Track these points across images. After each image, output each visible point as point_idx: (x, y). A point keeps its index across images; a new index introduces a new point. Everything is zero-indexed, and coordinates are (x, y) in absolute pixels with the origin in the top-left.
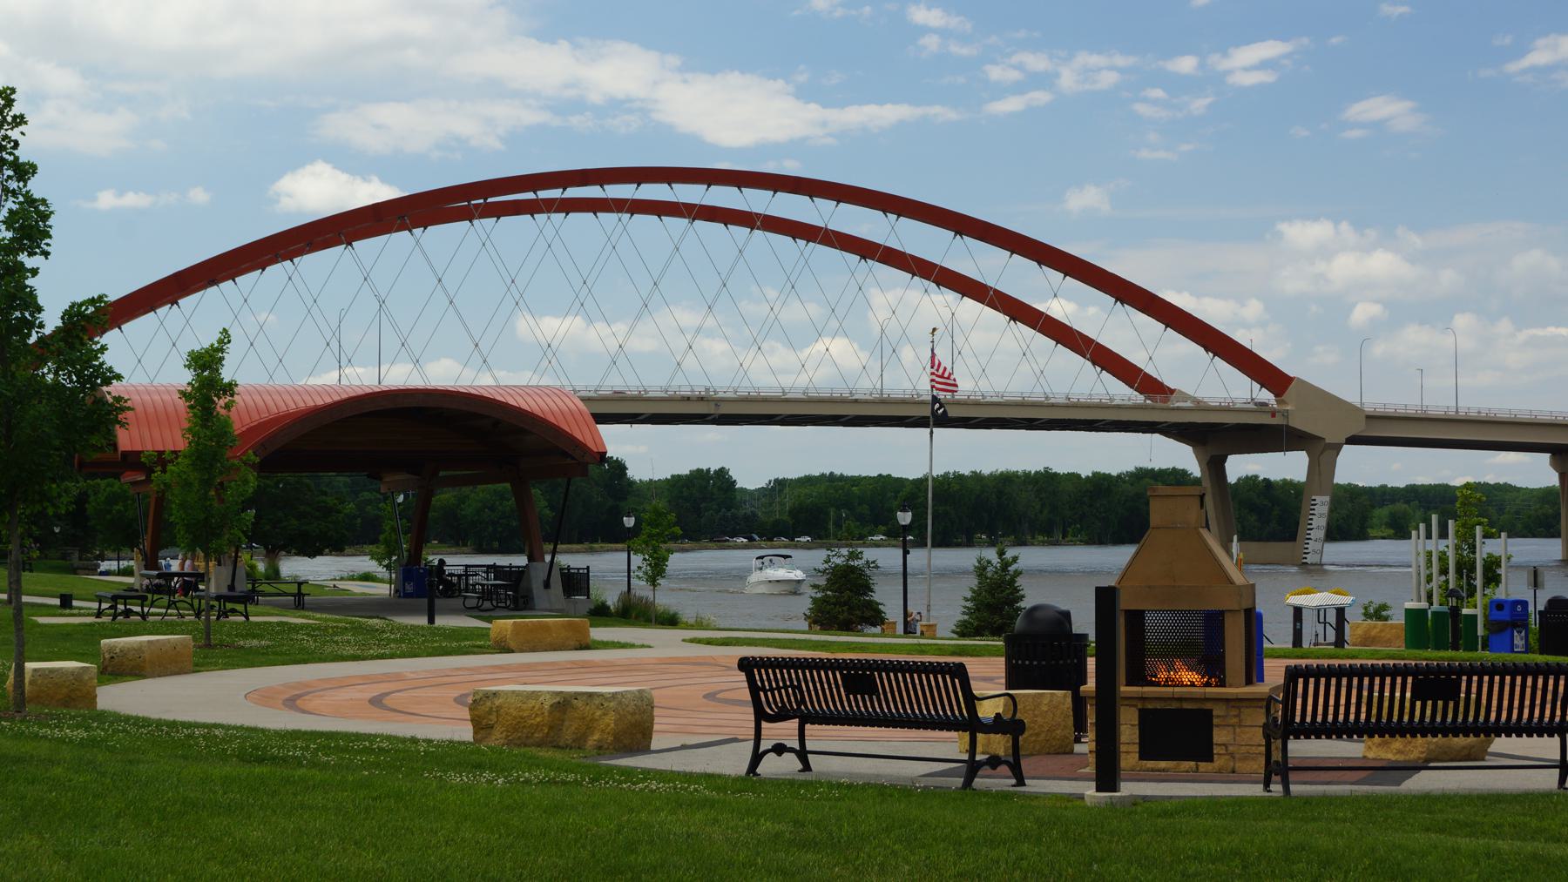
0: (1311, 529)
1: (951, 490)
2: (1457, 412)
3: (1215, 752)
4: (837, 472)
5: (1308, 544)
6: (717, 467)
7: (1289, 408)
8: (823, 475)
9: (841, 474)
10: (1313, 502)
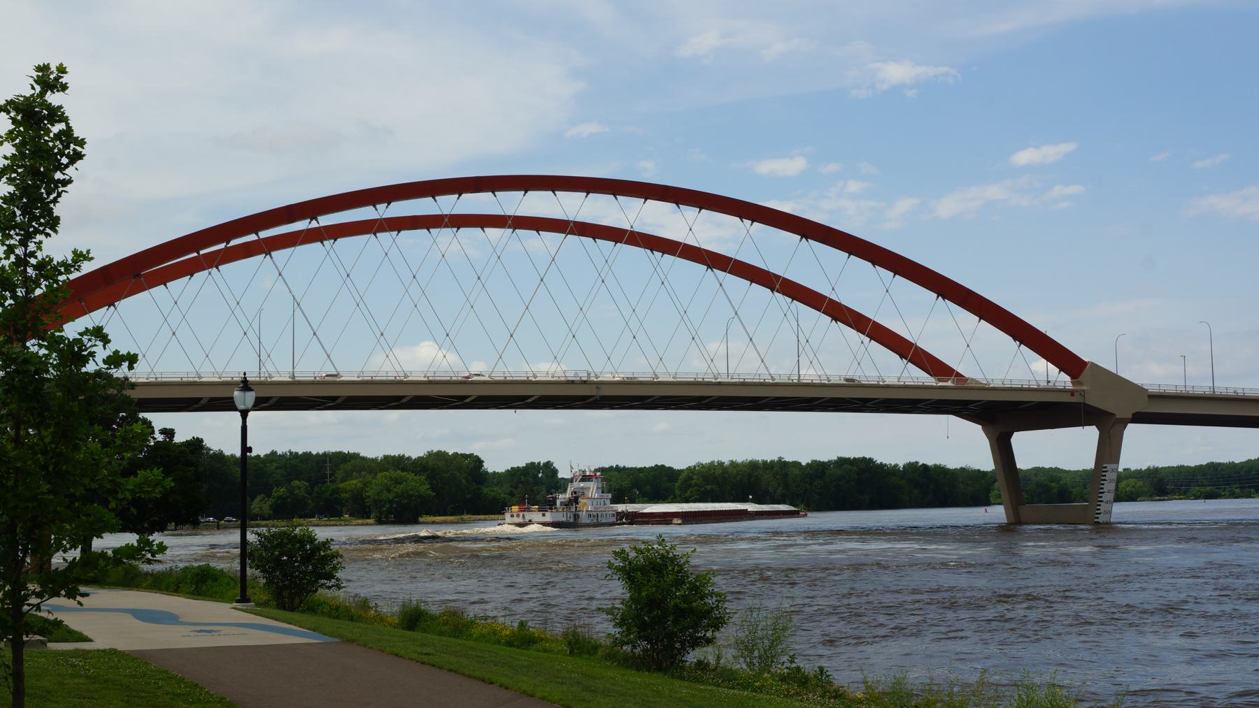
0: (1103, 493)
2: (1214, 391)
4: (621, 465)
5: (1100, 505)
6: (545, 461)
7: (1084, 388)
8: (612, 467)
9: (617, 466)
10: (1104, 470)
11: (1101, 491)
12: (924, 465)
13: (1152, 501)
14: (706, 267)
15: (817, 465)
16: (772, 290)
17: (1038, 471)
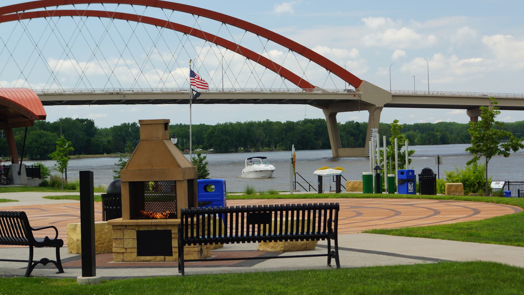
1: (228, 129)
2: (429, 93)
3: (173, 251)
7: (361, 93)
8: (177, 125)
9: (185, 124)
10: (371, 131)
12: (357, 123)
14: (183, 33)
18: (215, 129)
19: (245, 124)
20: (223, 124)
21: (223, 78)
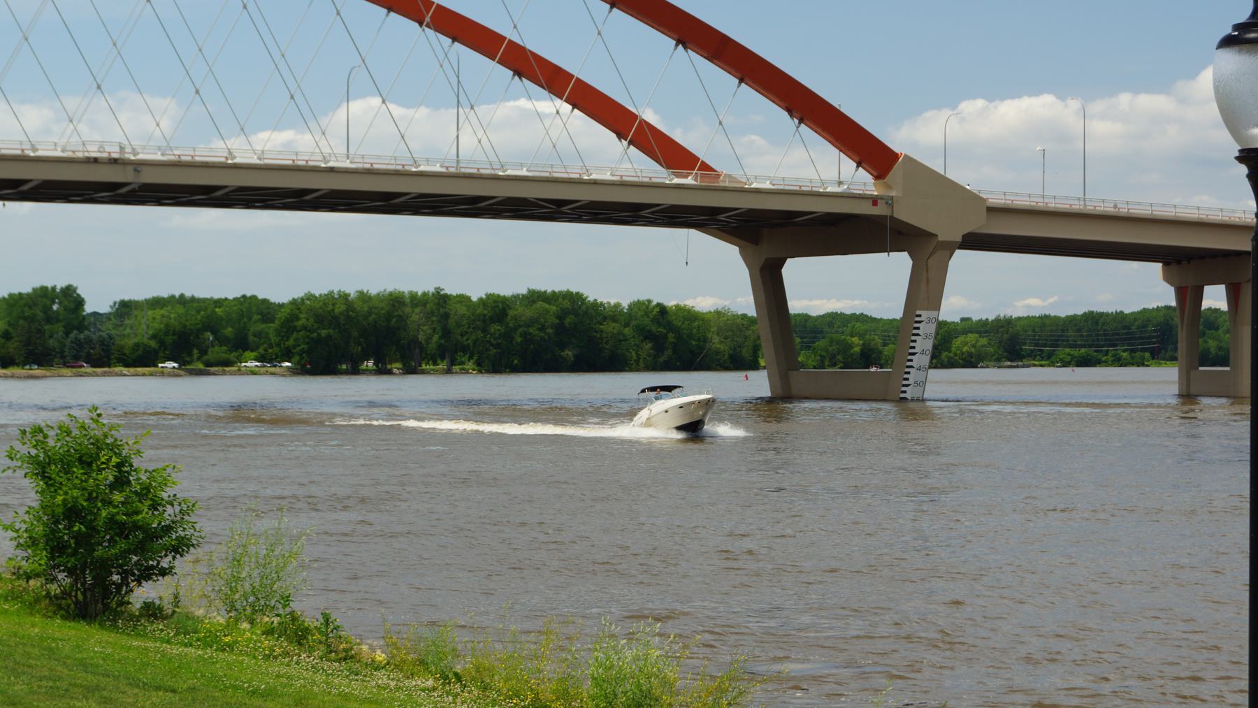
0: (914, 354)
4: (188, 294)
7: (893, 194)
8: (173, 297)
10: (917, 319)
11: (911, 351)
13: (999, 367)
15: (495, 302)
16: (421, 24)
17: (834, 318)
18: (299, 309)
19: (1068, 317)
20: (320, 295)
21: (458, 137)
